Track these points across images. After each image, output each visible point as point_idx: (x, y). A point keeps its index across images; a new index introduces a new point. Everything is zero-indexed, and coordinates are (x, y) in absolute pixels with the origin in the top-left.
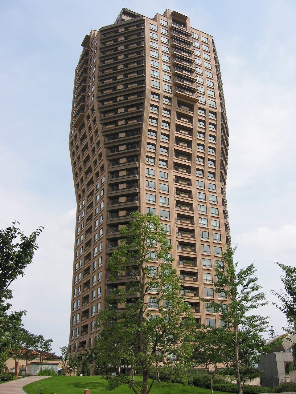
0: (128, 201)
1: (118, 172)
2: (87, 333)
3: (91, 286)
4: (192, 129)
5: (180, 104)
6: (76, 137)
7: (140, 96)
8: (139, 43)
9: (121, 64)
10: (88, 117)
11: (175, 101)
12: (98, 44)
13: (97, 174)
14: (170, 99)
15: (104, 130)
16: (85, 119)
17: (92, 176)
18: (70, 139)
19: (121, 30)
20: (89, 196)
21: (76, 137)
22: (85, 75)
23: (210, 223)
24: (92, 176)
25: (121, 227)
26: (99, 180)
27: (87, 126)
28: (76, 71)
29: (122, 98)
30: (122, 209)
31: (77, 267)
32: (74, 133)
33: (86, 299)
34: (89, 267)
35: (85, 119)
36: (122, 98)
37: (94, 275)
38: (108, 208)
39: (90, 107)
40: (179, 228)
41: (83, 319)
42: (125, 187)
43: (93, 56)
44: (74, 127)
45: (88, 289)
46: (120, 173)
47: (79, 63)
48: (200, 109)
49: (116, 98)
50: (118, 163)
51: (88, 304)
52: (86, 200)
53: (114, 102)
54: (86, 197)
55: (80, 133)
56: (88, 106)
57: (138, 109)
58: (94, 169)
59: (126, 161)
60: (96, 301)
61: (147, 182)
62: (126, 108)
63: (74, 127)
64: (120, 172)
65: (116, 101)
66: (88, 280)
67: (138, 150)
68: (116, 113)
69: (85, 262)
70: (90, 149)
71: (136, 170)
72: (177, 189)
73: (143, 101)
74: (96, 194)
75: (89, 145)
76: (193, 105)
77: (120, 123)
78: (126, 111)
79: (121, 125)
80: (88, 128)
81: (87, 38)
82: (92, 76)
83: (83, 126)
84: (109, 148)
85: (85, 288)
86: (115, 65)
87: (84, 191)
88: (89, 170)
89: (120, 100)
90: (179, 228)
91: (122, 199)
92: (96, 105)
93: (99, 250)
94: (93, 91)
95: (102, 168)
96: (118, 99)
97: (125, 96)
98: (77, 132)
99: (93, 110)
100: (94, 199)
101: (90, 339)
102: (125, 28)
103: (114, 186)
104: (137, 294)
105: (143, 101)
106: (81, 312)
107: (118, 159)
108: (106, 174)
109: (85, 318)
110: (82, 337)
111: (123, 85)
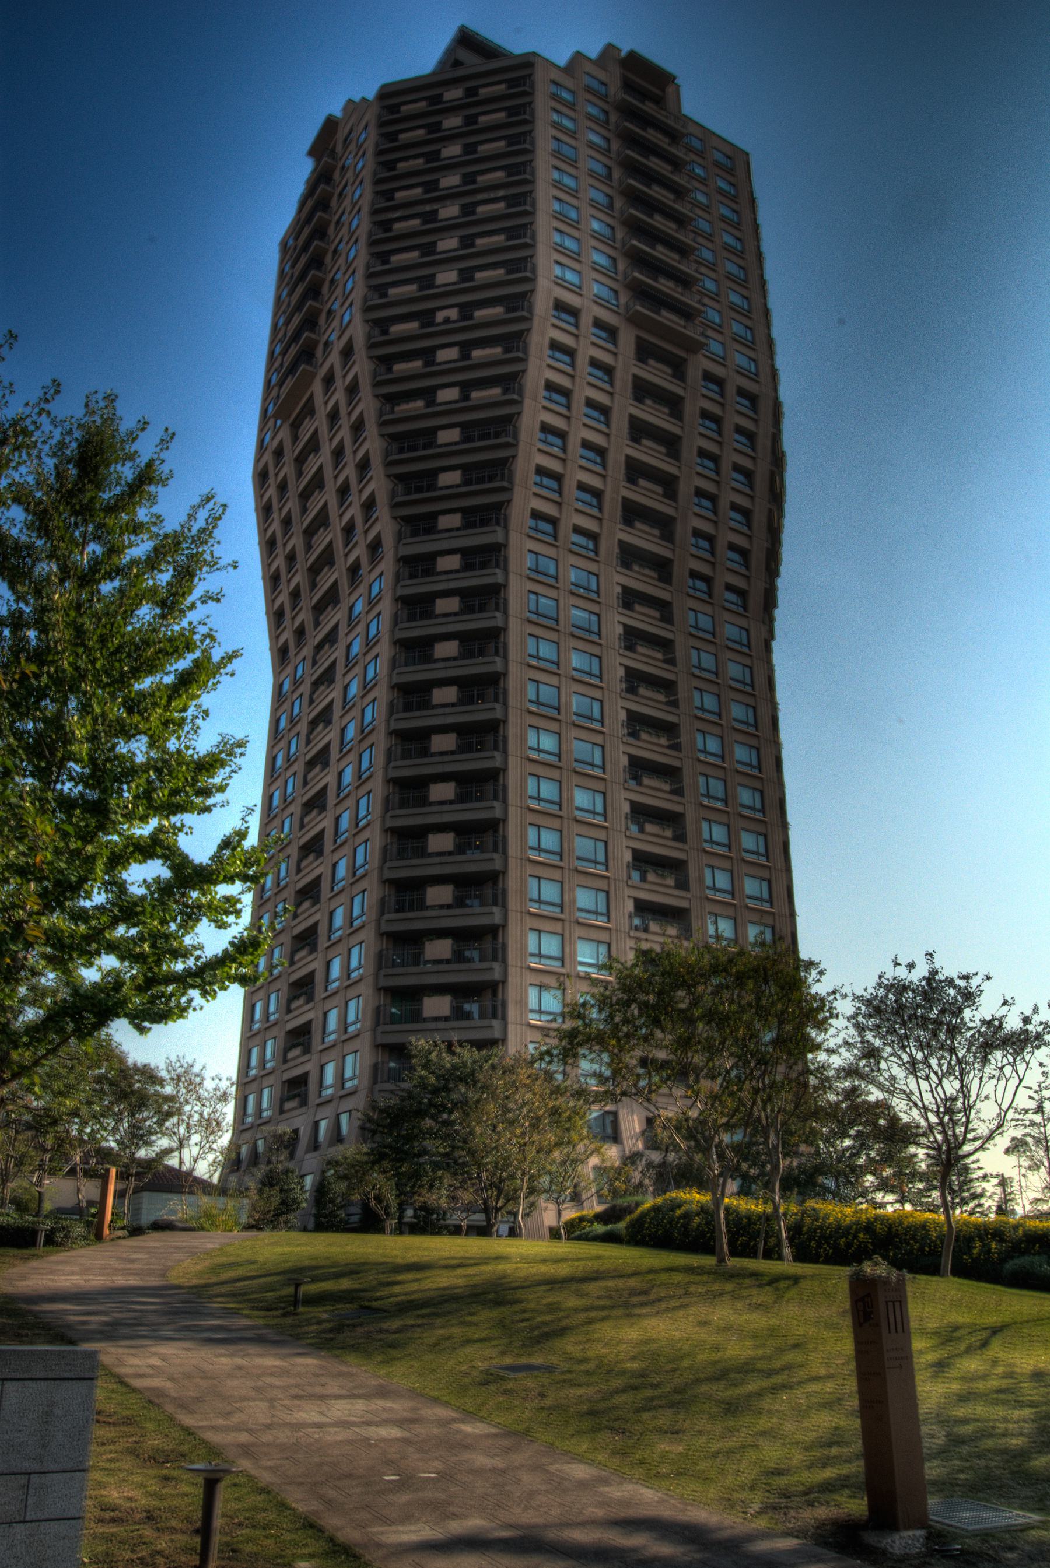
0: (462, 798)
1: (433, 557)
2: (304, 1103)
3: (317, 1045)
4: (679, 438)
5: (644, 352)
6: (279, 453)
7: (516, 309)
8: (512, 233)
9: (448, 202)
10: (329, 380)
11: (627, 338)
12: (369, 139)
13: (354, 570)
14: (612, 333)
15: (385, 418)
16: (317, 387)
17: (317, 917)
18: (257, 461)
19: (453, 94)
20: (319, 647)
21: (279, 453)
22: (317, 273)
23: (732, 752)
24: (317, 917)
25: (443, 605)
26: (362, 589)
27: (322, 411)
28: (284, 246)
29: (453, 353)
30: (441, 828)
31: (254, 1062)
32: (272, 439)
33: (300, 1037)
34: (317, 881)
35: (317, 387)
36: (453, 314)
37: (328, 1004)
38: (383, 922)
39: (339, 346)
40: (629, 712)
41: (288, 1105)
42: (453, 748)
43: (346, 239)
44: (276, 416)
45: (311, 952)
46: (439, 602)
47: (300, 210)
48: (708, 377)
49: (433, 311)
50: (429, 659)
51: (310, 1005)
52: (306, 697)
53: (423, 326)
54: (307, 651)
55: (295, 438)
56: (327, 344)
57: (507, 350)
58: (342, 553)
59: (457, 795)
60: (353, 795)
61: (533, 597)
62: (466, 387)
63: (276, 416)
64: (431, 837)
65: (432, 324)
66: (311, 922)
67: (503, 489)
68: (430, 362)
69: (296, 958)
70: (331, 487)
71: (493, 555)
72: (633, 421)
73: (526, 100)
74: (341, 717)
75: (328, 473)
76: (685, 360)
77: (443, 355)
78: (465, 397)
79: (446, 403)
80: (328, 415)
81: (330, 125)
82: (342, 305)
83: (309, 410)
84: (400, 478)
85: (298, 950)
86: (428, 208)
87: (300, 633)
88: (327, 559)
89: (447, 321)
90: (629, 712)
91: (441, 842)
92: (359, 331)
93: (347, 971)
94: (348, 321)
95: (375, 547)
96: (440, 316)
97: (461, 306)
98: (285, 434)
99: (347, 352)
100: (330, 778)
101: (316, 1124)
102: (461, 271)
103: (414, 606)
104: (491, 969)
105: (526, 100)
106: (283, 1034)
107: (434, 516)
108: (387, 565)
109: (297, 1051)
110: (285, 1116)
111: (430, 850)
